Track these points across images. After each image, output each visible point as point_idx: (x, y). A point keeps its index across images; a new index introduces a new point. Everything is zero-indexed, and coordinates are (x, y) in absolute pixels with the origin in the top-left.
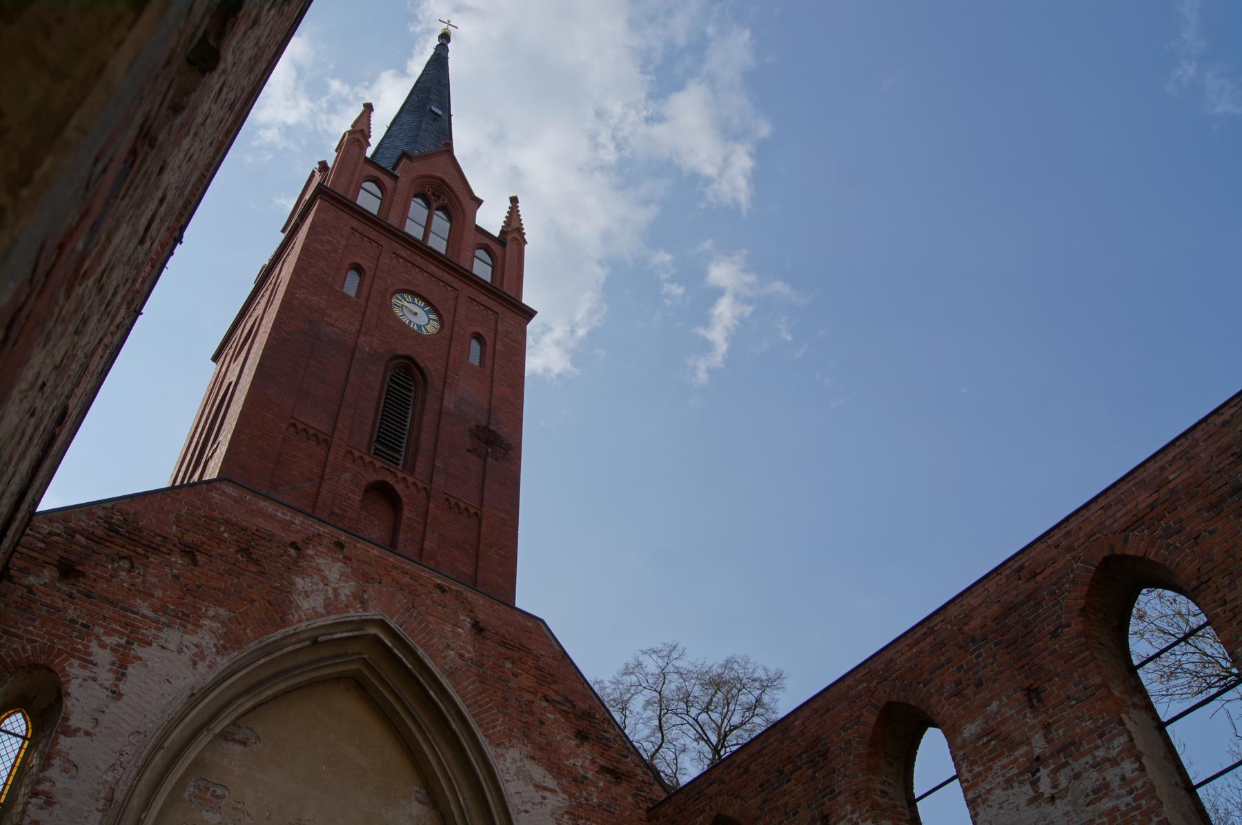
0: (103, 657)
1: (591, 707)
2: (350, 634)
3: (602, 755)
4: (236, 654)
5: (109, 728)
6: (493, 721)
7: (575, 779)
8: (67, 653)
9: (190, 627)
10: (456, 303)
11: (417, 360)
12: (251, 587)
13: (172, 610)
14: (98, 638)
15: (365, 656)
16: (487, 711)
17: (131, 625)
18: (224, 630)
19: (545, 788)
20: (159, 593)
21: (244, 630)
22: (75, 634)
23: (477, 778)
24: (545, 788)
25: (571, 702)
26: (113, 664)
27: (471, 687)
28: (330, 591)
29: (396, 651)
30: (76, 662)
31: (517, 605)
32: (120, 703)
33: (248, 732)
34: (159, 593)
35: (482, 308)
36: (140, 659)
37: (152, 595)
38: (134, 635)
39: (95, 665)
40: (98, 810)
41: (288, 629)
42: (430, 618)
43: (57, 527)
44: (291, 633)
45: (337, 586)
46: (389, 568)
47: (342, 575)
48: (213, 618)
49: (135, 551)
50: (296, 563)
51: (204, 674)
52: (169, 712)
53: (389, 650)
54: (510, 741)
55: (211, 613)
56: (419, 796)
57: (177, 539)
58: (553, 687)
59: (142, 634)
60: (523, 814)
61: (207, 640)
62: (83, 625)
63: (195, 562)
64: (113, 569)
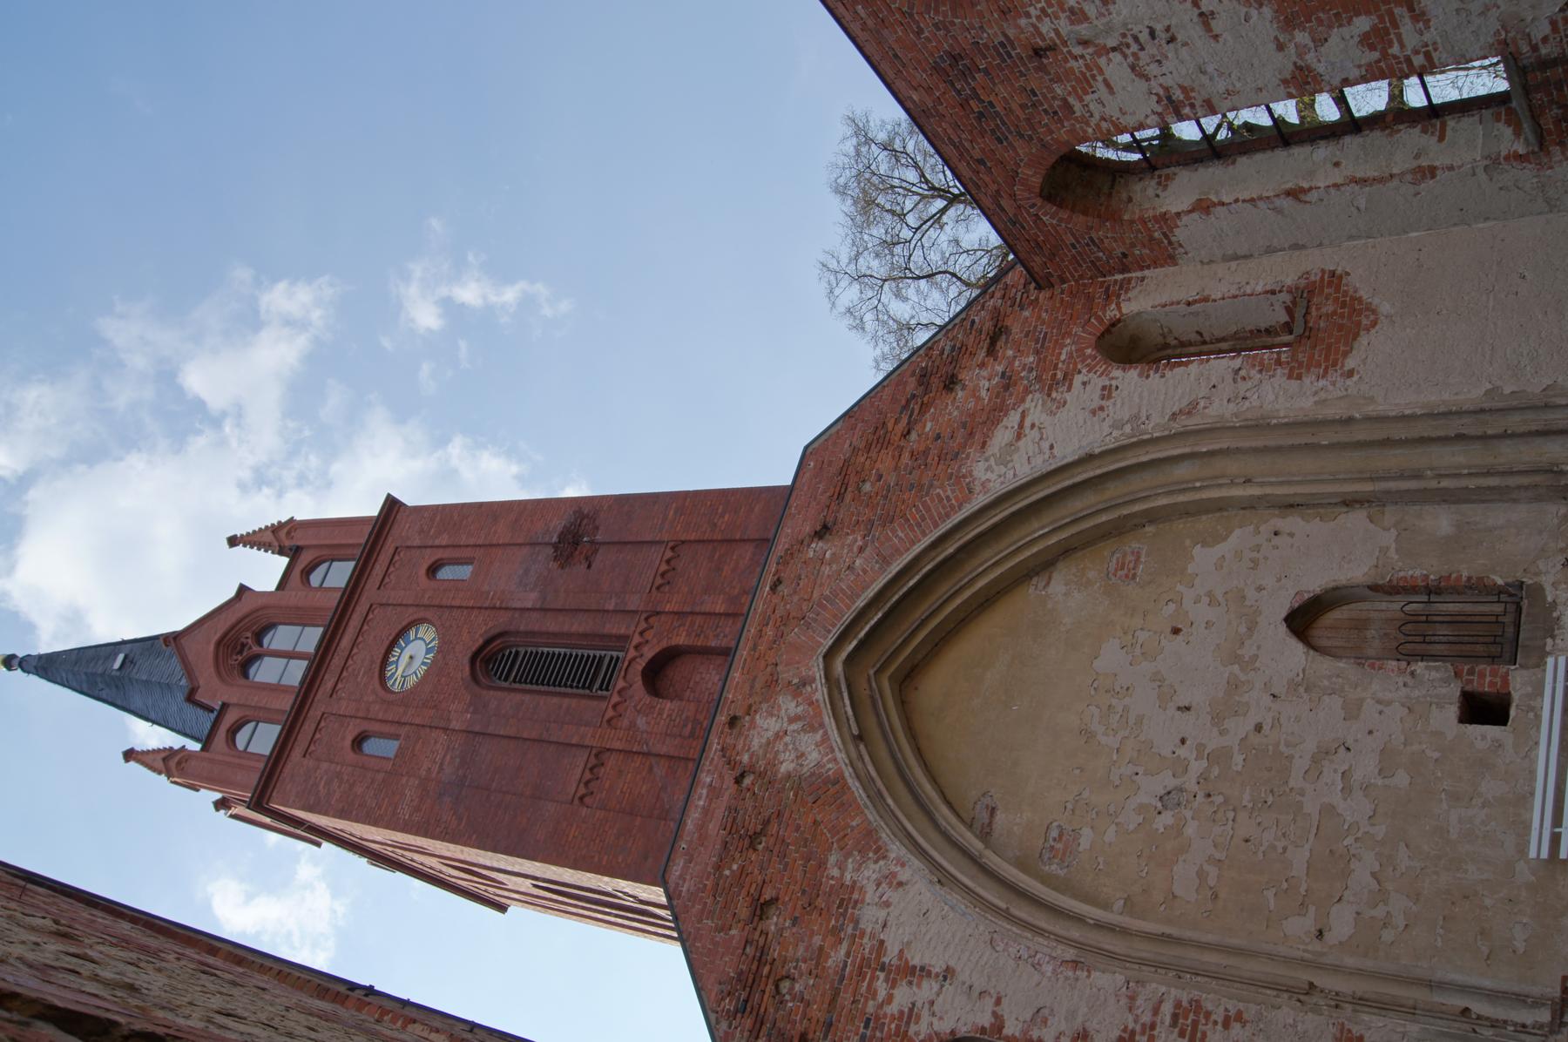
0: (903, 996)
1: (913, 374)
2: (846, 695)
3: (972, 354)
4: (884, 835)
5: (989, 977)
6: (940, 499)
7: (1006, 387)
9: (855, 896)
10: (389, 605)
11: (474, 649)
13: (837, 921)
14: (881, 1006)
15: (871, 672)
16: (928, 510)
17: (861, 967)
18: (856, 853)
19: (1021, 425)
21: (853, 829)
22: (878, 1034)
23: (1013, 514)
24: (1021, 425)
25: (908, 402)
26: (910, 983)
28: (794, 727)
29: (862, 634)
30: (913, 1028)
32: (958, 969)
33: (978, 807)
34: (817, 940)
35: (391, 569)
36: (901, 951)
37: (821, 948)
38: (872, 963)
39: (913, 1004)
40: (1088, 977)
41: (847, 774)
42: (816, 595)
44: (851, 770)
45: (786, 719)
46: (757, 655)
47: (772, 715)
48: (841, 867)
49: (768, 977)
50: (761, 775)
51: (913, 871)
52: (963, 907)
54: (964, 476)
55: (835, 872)
57: (747, 928)
58: (890, 425)
60: (1055, 451)
61: (871, 872)
62: (866, 1027)
64: (793, 1000)
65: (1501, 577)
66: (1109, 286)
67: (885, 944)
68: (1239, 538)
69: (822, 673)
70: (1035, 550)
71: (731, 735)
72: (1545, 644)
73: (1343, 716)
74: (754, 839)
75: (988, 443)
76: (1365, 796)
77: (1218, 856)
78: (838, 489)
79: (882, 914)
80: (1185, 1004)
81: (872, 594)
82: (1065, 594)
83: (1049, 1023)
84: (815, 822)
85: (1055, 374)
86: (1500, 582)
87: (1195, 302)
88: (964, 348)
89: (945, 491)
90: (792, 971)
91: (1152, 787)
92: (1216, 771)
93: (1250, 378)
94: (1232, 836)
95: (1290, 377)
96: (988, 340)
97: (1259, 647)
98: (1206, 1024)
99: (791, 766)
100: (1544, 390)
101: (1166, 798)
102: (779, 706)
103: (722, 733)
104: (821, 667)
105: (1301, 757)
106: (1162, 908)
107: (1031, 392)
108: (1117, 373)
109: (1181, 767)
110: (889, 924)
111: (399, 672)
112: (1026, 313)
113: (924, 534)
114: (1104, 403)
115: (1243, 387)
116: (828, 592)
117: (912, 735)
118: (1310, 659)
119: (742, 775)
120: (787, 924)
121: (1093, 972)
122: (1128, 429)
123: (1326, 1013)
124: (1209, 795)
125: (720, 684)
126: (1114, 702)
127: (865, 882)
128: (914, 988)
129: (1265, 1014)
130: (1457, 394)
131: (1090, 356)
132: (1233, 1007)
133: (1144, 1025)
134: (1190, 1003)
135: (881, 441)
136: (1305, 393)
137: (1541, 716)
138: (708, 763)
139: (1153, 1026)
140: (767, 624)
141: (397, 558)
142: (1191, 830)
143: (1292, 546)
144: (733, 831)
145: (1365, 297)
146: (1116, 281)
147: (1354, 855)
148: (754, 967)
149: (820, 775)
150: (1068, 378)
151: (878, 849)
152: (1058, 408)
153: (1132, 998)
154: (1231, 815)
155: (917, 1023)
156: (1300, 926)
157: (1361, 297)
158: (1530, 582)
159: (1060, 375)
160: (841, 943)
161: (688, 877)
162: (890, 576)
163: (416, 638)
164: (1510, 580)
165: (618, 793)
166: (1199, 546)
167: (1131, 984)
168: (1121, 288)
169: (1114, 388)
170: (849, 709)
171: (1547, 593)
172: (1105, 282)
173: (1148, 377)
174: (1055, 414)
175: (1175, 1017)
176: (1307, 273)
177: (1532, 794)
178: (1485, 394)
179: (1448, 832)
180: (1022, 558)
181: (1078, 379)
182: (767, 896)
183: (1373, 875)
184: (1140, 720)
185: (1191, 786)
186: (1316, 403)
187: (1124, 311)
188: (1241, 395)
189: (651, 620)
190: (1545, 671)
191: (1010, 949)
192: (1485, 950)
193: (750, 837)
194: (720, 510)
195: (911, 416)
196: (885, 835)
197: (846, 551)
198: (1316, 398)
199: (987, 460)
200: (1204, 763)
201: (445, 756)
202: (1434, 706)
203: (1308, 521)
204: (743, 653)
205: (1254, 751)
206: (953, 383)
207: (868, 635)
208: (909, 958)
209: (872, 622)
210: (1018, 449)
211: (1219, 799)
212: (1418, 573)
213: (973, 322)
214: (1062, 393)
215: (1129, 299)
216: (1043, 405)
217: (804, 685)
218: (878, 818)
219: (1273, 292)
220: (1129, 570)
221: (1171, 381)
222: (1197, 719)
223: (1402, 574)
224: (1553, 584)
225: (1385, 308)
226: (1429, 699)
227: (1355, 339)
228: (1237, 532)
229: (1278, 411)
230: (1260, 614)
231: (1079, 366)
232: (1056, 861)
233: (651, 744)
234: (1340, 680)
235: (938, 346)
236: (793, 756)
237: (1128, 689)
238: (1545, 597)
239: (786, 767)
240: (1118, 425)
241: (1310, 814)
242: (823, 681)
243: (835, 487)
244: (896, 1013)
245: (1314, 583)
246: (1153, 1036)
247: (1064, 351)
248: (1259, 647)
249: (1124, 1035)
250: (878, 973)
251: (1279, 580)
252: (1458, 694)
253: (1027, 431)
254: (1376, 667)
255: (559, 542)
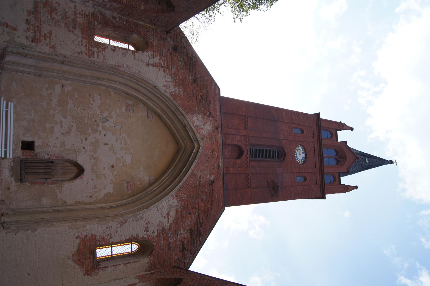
0: (157, 60)
1: (203, 235)
2: (192, 137)
5: (138, 64)
6: (184, 193)
8: (154, 50)
9: (174, 84)
11: (286, 157)
12: (192, 100)
13: (176, 78)
14: (161, 58)
15: (187, 147)
18: (177, 94)
19: (168, 217)
20: (180, 74)
21: (180, 101)
22: (160, 52)
24: (168, 217)
25: (201, 226)
26: (156, 63)
27: (192, 183)
28: (201, 127)
29: (193, 154)
30: (152, 53)
31: (226, 208)
33: (152, 117)
36: (160, 70)
37: (178, 72)
38: (166, 68)
39: (153, 58)
40: (115, 64)
41: (185, 114)
42: (208, 164)
43: (185, 44)
45: (204, 129)
46: (217, 146)
47: (208, 130)
48: (179, 91)
49: (188, 65)
50: (206, 114)
51: (163, 89)
52: (148, 80)
53: (192, 152)
54: (179, 201)
55: (180, 90)
56: (151, 180)
58: (204, 218)
59: (167, 70)
60: (157, 209)
61: (172, 89)
62: (163, 54)
63: (192, 84)
64: (181, 60)
65: (27, 184)
66: (155, 269)
67: (164, 72)
68: (101, 195)
69: (199, 142)
70: (155, 185)
71: (216, 125)
72: (13, 164)
73: (65, 143)
74: (202, 98)
75: (176, 212)
76: (56, 121)
77: (91, 105)
78: (212, 196)
79: (166, 79)
80: (92, 57)
81: (194, 164)
82: (144, 177)
83: (122, 53)
84: (189, 102)
85: (163, 235)
86: (27, 183)
87: (128, 263)
88: (191, 244)
89: (183, 196)
90: (183, 67)
91: (110, 123)
92: (95, 127)
93: (106, 235)
94: (88, 110)
95: (95, 235)
96: (185, 247)
97: (90, 162)
98: (86, 52)
99: (199, 116)
100: (19, 231)
101: (106, 120)
102: (207, 132)
103: (218, 126)
104: (200, 143)
105: (74, 131)
106: (102, 92)
107: (168, 229)
108: (145, 236)
109: (104, 128)
110: (164, 77)
111: (301, 150)
112: (176, 257)
113: (185, 182)
114: (147, 226)
115: (108, 232)
116: (205, 164)
117: (173, 135)
118: (76, 159)
119: (210, 115)
120: (187, 77)
121: (115, 64)
122: (138, 217)
123: (59, 54)
124: (96, 121)
125: (224, 152)
126: (124, 146)
127: (173, 87)
128: (154, 62)
129: (73, 54)
130: (45, 230)
131: (155, 242)
132: (80, 56)
133: (100, 52)
134: (91, 57)
135: (205, 212)
136: (90, 230)
137: (13, 143)
138: (219, 118)
139: (98, 52)
140: (217, 155)
141: (315, 182)
142: (98, 112)
143: (86, 193)
144: (207, 100)
145: (77, 266)
146: (153, 270)
147: (57, 105)
148: (192, 68)
149: (191, 114)
150: (159, 235)
151: (172, 95)
152: (159, 224)
153: (104, 58)
154: (89, 116)
155: (152, 54)
156: (68, 88)
157: (78, 266)
158: (19, 183)
159: (161, 235)
160: (174, 73)
161: (214, 89)
162: (190, 169)
163: (301, 160)
164: (24, 184)
165: (238, 120)
166: (111, 193)
167: (105, 61)
168: (151, 267)
169: (145, 231)
170: (190, 133)
171: (14, 180)
172: (156, 270)
173: (136, 235)
174: (160, 221)
175: (94, 54)
176: (96, 275)
177: (14, 122)
178: (37, 230)
179: (34, 112)
180: (158, 183)
181: (156, 234)
182: (194, 84)
183: (52, 101)
184: (117, 141)
185: (100, 123)
186: (86, 226)
187: (148, 259)
188: (108, 229)
189: (247, 166)
190: (13, 156)
191: (135, 70)
192: (22, 82)
193: (203, 99)
194: (241, 199)
195: (199, 220)
196: (171, 98)
197: (204, 177)
198: (86, 228)
199: (175, 206)
200: (98, 129)
201: (281, 128)
202: (41, 146)
203: (83, 201)
204: (220, 147)
205: (86, 133)
206: (191, 233)
207: (191, 154)
208: (157, 69)
209: (191, 158)
210: (167, 209)
211: (93, 120)
212: (50, 186)
213: (191, 254)
214: (159, 229)
215: (148, 263)
216: (164, 225)
217: (203, 138)
218: (174, 103)
219: (106, 267)
220: (129, 185)
221: (129, 233)
222: (102, 141)
223: (55, 185)
224: (12, 182)
225: (70, 261)
226: (43, 148)
227: (78, 249)
228: (102, 197)
229: (96, 224)
230: (91, 172)
231: (157, 238)
232: (130, 104)
233: (235, 132)
234: (67, 153)
235: (198, 245)
236: (199, 119)
237: (122, 149)
238: (14, 179)
239: (200, 116)
240: (141, 218)
241: (70, 116)
242: (198, 139)
243: (213, 197)
244: (157, 57)
245: (78, 181)
246: (98, 50)
247: (162, 244)
248: (90, 162)
249: (104, 50)
250: (164, 66)
251: (88, 182)
252: (35, 149)
253: (166, 216)
254: (58, 157)
255: (278, 188)
